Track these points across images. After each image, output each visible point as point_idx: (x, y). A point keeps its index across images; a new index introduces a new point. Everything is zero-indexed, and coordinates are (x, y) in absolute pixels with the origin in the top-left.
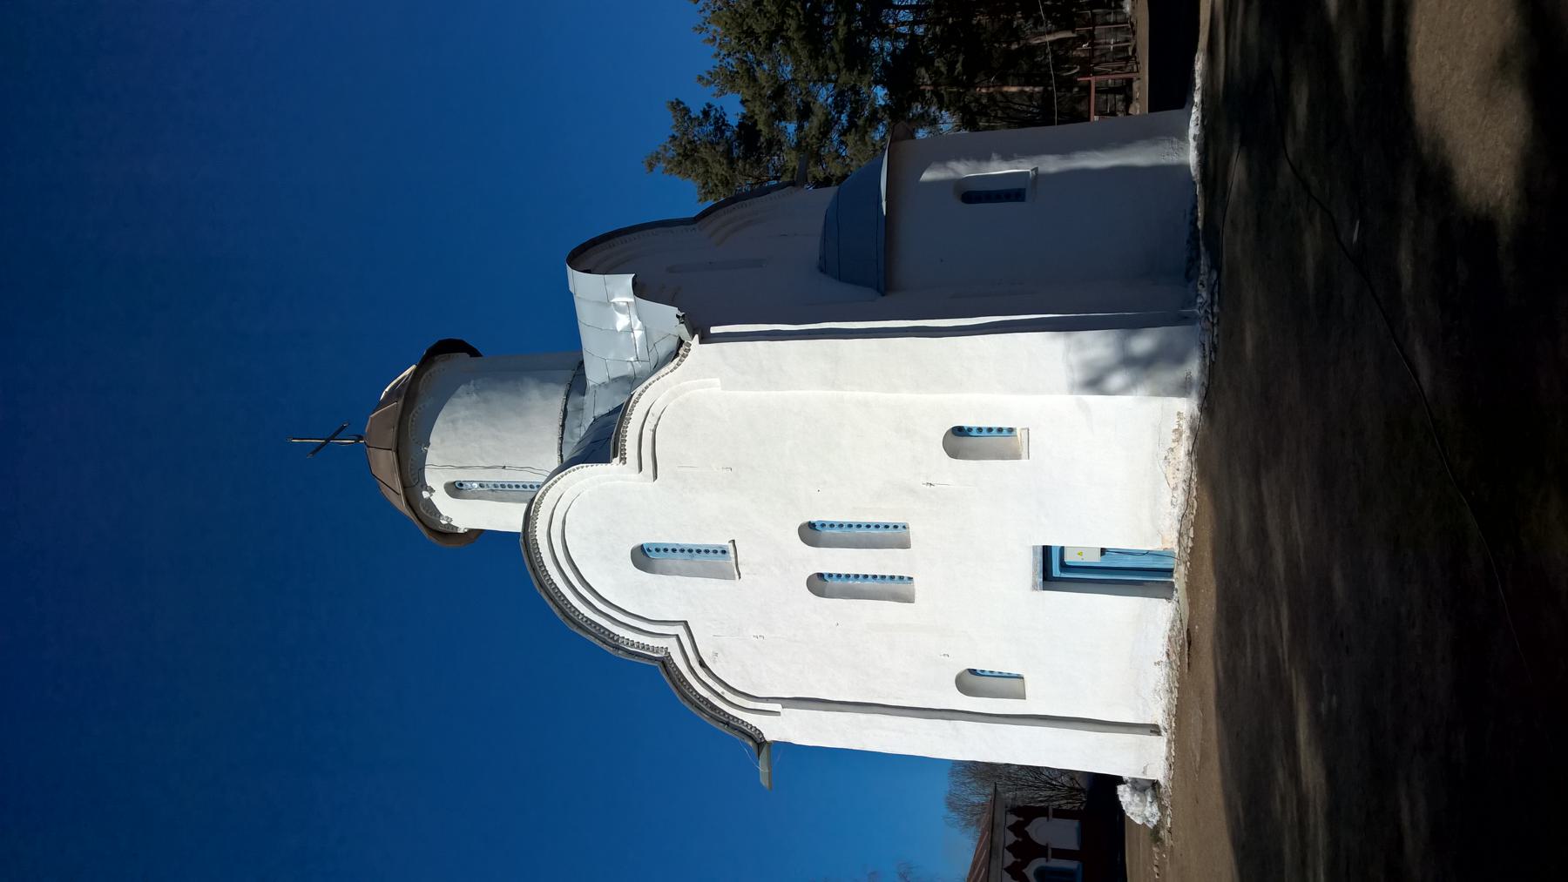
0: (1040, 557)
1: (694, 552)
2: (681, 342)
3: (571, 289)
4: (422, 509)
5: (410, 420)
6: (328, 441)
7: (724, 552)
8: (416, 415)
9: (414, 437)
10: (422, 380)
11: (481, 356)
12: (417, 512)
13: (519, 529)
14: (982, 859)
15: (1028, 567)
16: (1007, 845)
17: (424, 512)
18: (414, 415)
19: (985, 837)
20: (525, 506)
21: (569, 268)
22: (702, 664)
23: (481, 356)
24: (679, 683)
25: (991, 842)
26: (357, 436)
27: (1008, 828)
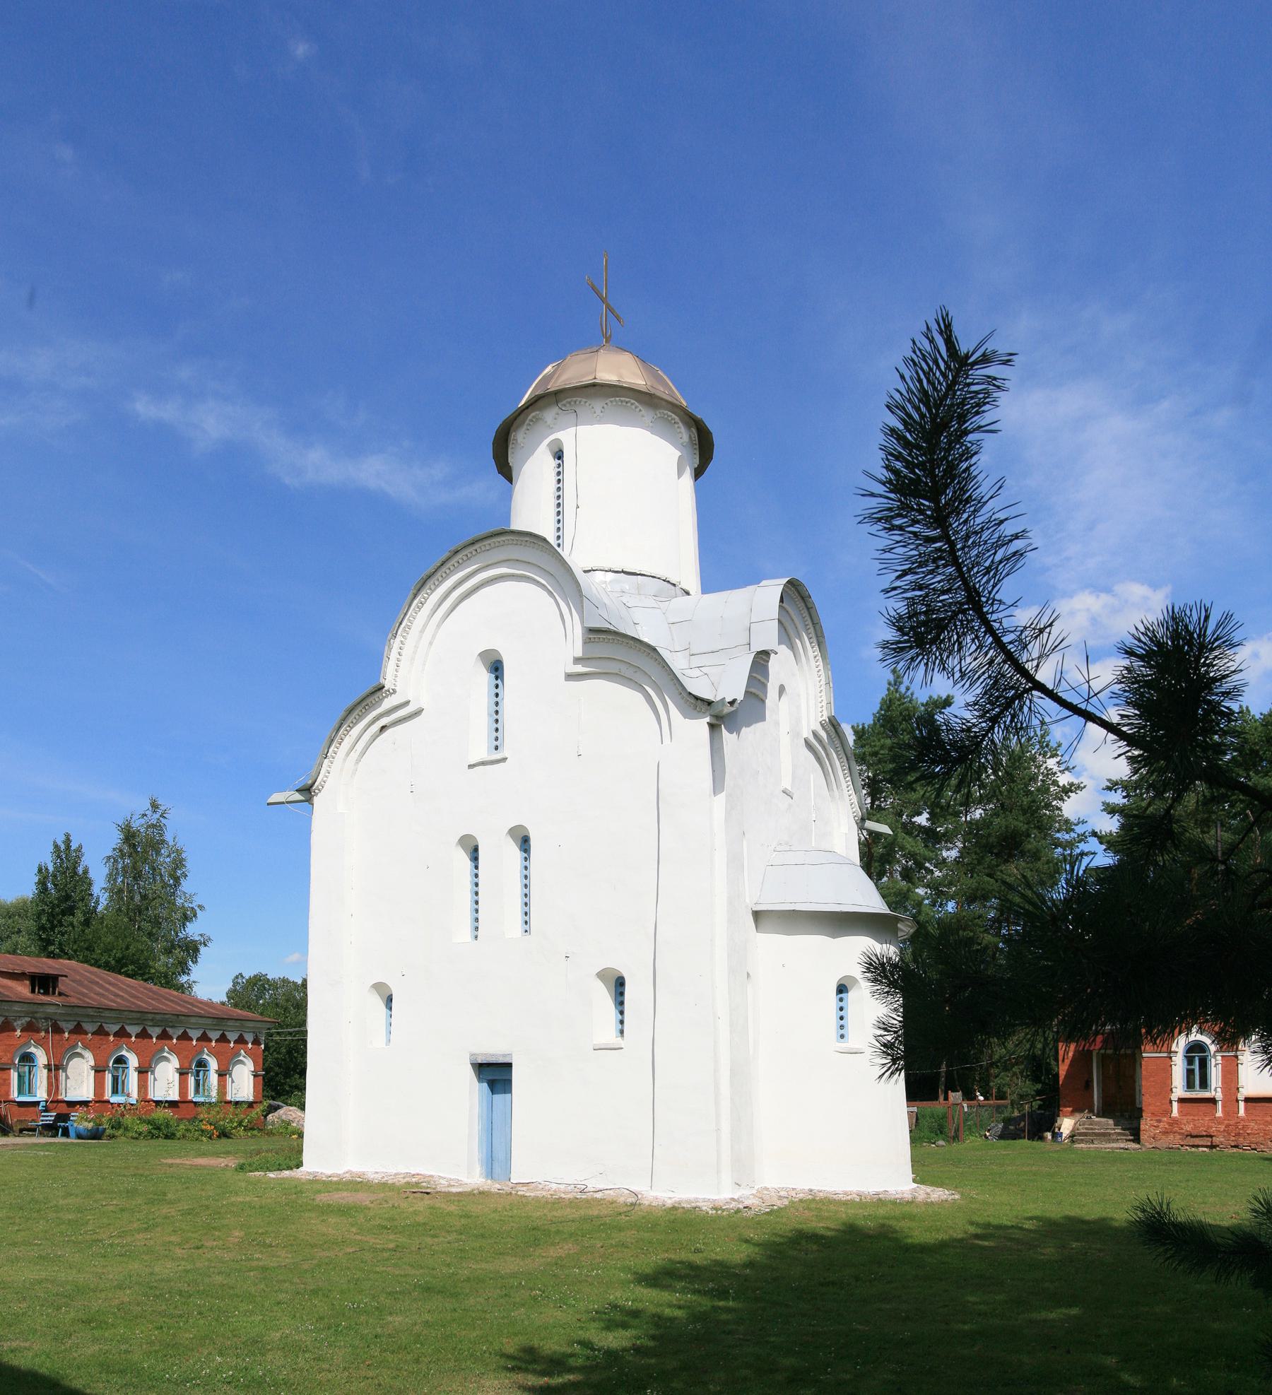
0: (501, 1060)
1: (496, 717)
2: (709, 703)
3: (764, 583)
4: (533, 414)
5: (627, 400)
6: (603, 300)
7: (496, 748)
8: (633, 407)
9: (610, 404)
10: (670, 413)
11: (679, 478)
12: (529, 409)
13: (516, 526)
14: (194, 1009)
15: (493, 1050)
16: (226, 1033)
17: (530, 417)
18: (632, 404)
19: (179, 1008)
20: (1050, 686)
21: (785, 581)
22: (383, 728)
23: (679, 478)
24: (363, 704)
25: (228, 1019)
26: (611, 336)
27: (101, 1026)
